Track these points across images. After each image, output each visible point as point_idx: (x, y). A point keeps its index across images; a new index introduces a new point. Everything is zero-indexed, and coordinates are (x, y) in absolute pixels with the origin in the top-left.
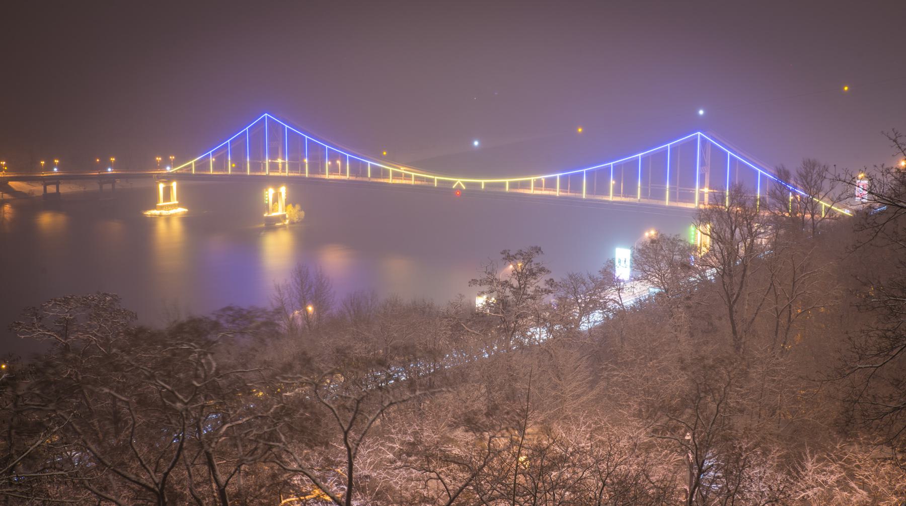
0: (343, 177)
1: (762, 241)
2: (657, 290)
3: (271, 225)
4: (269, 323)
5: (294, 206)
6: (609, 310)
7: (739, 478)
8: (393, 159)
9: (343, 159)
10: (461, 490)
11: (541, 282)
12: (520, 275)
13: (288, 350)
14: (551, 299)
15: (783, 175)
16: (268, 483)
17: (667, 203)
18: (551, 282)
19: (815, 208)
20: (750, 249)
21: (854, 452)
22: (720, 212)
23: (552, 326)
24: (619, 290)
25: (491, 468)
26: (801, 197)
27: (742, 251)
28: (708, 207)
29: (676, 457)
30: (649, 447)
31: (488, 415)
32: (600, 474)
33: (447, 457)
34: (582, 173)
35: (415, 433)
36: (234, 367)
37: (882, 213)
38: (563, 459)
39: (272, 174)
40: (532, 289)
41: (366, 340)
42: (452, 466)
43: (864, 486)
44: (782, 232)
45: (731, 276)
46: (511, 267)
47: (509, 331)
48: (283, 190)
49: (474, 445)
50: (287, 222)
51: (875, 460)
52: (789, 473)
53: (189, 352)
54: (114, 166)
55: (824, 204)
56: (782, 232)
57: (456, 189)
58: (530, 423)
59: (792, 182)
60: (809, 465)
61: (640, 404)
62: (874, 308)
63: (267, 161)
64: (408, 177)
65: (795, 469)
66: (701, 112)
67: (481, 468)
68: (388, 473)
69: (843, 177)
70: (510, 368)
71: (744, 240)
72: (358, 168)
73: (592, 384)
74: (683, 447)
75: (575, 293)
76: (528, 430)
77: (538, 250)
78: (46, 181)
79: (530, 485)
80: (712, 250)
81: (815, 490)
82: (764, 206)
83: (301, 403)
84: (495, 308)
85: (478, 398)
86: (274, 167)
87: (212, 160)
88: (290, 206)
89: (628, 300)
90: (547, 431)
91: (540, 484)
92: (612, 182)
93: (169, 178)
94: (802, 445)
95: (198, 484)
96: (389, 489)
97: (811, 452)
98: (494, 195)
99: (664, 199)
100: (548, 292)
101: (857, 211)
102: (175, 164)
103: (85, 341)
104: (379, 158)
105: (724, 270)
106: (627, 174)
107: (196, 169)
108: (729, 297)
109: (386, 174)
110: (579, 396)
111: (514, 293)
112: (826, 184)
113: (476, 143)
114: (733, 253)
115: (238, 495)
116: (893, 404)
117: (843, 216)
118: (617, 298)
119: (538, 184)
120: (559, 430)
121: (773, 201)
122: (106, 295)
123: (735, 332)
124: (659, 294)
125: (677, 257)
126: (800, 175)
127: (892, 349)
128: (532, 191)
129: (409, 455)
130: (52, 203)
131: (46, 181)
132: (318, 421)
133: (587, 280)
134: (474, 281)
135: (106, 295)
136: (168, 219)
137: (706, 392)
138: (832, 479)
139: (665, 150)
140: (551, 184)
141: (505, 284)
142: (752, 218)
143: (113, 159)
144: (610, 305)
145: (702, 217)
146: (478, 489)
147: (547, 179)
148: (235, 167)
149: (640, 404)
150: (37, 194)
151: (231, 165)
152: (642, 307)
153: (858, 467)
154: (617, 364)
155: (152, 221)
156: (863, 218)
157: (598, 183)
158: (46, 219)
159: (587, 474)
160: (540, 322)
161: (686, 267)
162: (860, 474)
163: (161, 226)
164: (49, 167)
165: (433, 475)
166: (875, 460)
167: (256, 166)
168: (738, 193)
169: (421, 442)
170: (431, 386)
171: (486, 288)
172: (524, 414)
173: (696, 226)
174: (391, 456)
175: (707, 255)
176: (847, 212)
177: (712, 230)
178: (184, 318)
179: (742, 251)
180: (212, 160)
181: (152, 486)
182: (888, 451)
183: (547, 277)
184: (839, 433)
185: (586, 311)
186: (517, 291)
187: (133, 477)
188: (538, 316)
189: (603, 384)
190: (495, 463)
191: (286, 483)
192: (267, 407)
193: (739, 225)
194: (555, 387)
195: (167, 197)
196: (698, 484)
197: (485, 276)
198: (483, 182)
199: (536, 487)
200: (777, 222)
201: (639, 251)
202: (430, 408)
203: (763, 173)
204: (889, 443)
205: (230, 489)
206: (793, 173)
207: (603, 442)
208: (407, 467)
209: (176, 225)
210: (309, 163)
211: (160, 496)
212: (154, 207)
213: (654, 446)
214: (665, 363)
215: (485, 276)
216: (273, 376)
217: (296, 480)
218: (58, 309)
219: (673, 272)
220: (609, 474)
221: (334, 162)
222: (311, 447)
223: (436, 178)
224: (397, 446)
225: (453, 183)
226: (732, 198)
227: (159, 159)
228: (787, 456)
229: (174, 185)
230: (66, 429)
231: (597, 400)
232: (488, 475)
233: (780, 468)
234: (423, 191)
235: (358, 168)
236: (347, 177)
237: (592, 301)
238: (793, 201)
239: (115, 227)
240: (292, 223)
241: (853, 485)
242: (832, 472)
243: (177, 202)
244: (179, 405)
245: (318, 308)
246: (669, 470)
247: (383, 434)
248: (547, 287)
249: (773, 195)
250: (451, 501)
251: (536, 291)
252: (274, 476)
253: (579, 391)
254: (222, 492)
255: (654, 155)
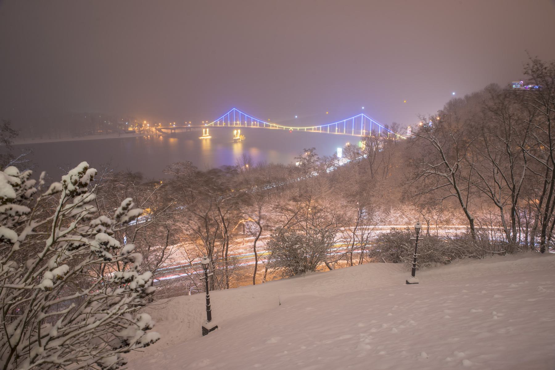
0: (257, 127)
1: (380, 146)
2: (349, 161)
3: (236, 141)
4: (235, 170)
5: (242, 136)
6: (335, 167)
7: (372, 215)
8: (271, 122)
9: (257, 122)
10: (291, 219)
11: (315, 158)
12: (309, 156)
13: (241, 178)
14: (318, 163)
15: (386, 127)
16: (236, 216)
17: (353, 135)
18: (318, 158)
19: (395, 137)
20: (377, 149)
21: (405, 207)
22: (368, 138)
23: (318, 171)
24: (338, 160)
25: (301, 212)
26: (392, 133)
27: (374, 149)
28: (365, 136)
29: (354, 209)
30: (346, 206)
31: (299, 197)
32: (332, 214)
33: (288, 209)
34: (328, 126)
35: (278, 202)
36: (225, 183)
37: (415, 138)
38: (322, 210)
39: (236, 126)
40: (313, 160)
41: (264, 175)
42: (289, 211)
43: (407, 217)
44: (386, 144)
45: (371, 157)
46: (307, 154)
47: (306, 173)
48: (239, 131)
49: (295, 206)
50: (240, 140)
51: (410, 210)
52: (386, 214)
53: (213, 178)
54: (191, 124)
55: (398, 136)
56: (386, 144)
57: (290, 131)
58: (312, 199)
59: (389, 129)
60: (392, 211)
61: (344, 194)
62: (412, 166)
63: (235, 122)
64: (276, 127)
65: (388, 212)
66: (363, 108)
67: (297, 212)
68: (270, 214)
69: (404, 127)
70: (306, 183)
71: (375, 146)
72: (261, 124)
73: (330, 188)
74: (357, 206)
75: (325, 161)
76: (311, 201)
77: (314, 149)
78: (172, 129)
79: (312, 217)
80: (366, 149)
81: (393, 218)
82: (381, 136)
83: (245, 194)
84: (302, 166)
85: (296, 192)
86: (236, 124)
87: (218, 122)
88: (241, 136)
89: (341, 164)
90: (317, 201)
91: (315, 217)
92: (337, 128)
93: (206, 128)
94: (390, 206)
95: (216, 216)
96: (271, 218)
97: (393, 207)
98: (302, 132)
99: (352, 133)
100: (317, 161)
101: (408, 138)
102: (208, 123)
103: (183, 175)
104: (267, 121)
105: (369, 155)
106: (341, 126)
107: (214, 125)
108: (370, 163)
109: (269, 126)
110: (326, 192)
111: (307, 161)
112: (399, 129)
113: (296, 117)
114: (372, 150)
115: (227, 219)
116: (416, 194)
117: (404, 139)
118: (338, 163)
119: (315, 129)
120: (320, 201)
121: (384, 134)
122: (189, 162)
123: (372, 173)
124: (350, 162)
125: (356, 151)
126: (392, 127)
127: (417, 178)
128: (313, 131)
129: (277, 208)
130: (173, 135)
131: (172, 129)
132: (250, 199)
133: (329, 158)
134: (295, 158)
135: (189, 162)
136: (206, 139)
137: (363, 191)
138: (398, 215)
139: (352, 119)
140: (318, 129)
141: (305, 159)
142: (377, 139)
143: (190, 122)
144: (336, 165)
145: (363, 139)
146: (296, 218)
147: (317, 128)
148: (192, 122)
149: (344, 194)
150: (169, 133)
151: (224, 124)
152: (345, 166)
153: (405, 211)
154: (337, 182)
155: (201, 140)
156: (409, 140)
157: (333, 128)
158: (172, 140)
159: (328, 214)
160: (315, 170)
161: (358, 154)
162: (406, 214)
163: (204, 142)
164: (172, 125)
165: (283, 214)
166: (410, 210)
167: (231, 124)
168: (373, 132)
169: (280, 205)
170: (283, 189)
171: (299, 160)
172: (310, 197)
173: (361, 142)
174: (271, 209)
175: (364, 150)
176: (405, 138)
177: (366, 143)
178: (210, 168)
179: (374, 149)
180: (218, 122)
181: (203, 216)
182: (414, 207)
183: (317, 157)
184: (401, 202)
185: (328, 167)
186: (308, 161)
187: (198, 214)
188: (314, 168)
189: (333, 188)
190: (301, 211)
191: (241, 216)
192: (235, 194)
193: (374, 141)
194: (319, 189)
195: (206, 133)
196: (360, 217)
197: (299, 156)
198: (298, 128)
199: (314, 218)
200: (385, 141)
201: (344, 149)
202: (282, 195)
203: (381, 126)
204: (414, 205)
205: (225, 218)
206: (390, 126)
207: (333, 205)
208: (276, 212)
209: (208, 141)
210: (247, 123)
211: (206, 219)
212: (202, 136)
213: (348, 206)
214: (351, 182)
215: (299, 156)
216: (237, 186)
217: (244, 215)
218: (175, 166)
219: (354, 155)
220: (335, 214)
221: (254, 122)
222: (248, 206)
223: (284, 127)
224: (273, 206)
225: (304, 129)
226: (372, 134)
227: (203, 122)
228: (386, 209)
229: (208, 130)
230: (179, 200)
231: (332, 193)
232: (299, 214)
233: (384, 212)
234: (281, 131)
235: (261, 124)
236: (258, 127)
237: (330, 164)
238: (389, 135)
239: (191, 142)
240: (242, 141)
241: (404, 216)
242: (398, 213)
243: (208, 135)
244: (210, 194)
245: (249, 166)
246: (352, 213)
247: (269, 202)
248: (317, 159)
249: (384, 133)
250: (289, 222)
251: (314, 161)
252: (238, 214)
253: (326, 190)
254: (223, 218)
255: (349, 121)
